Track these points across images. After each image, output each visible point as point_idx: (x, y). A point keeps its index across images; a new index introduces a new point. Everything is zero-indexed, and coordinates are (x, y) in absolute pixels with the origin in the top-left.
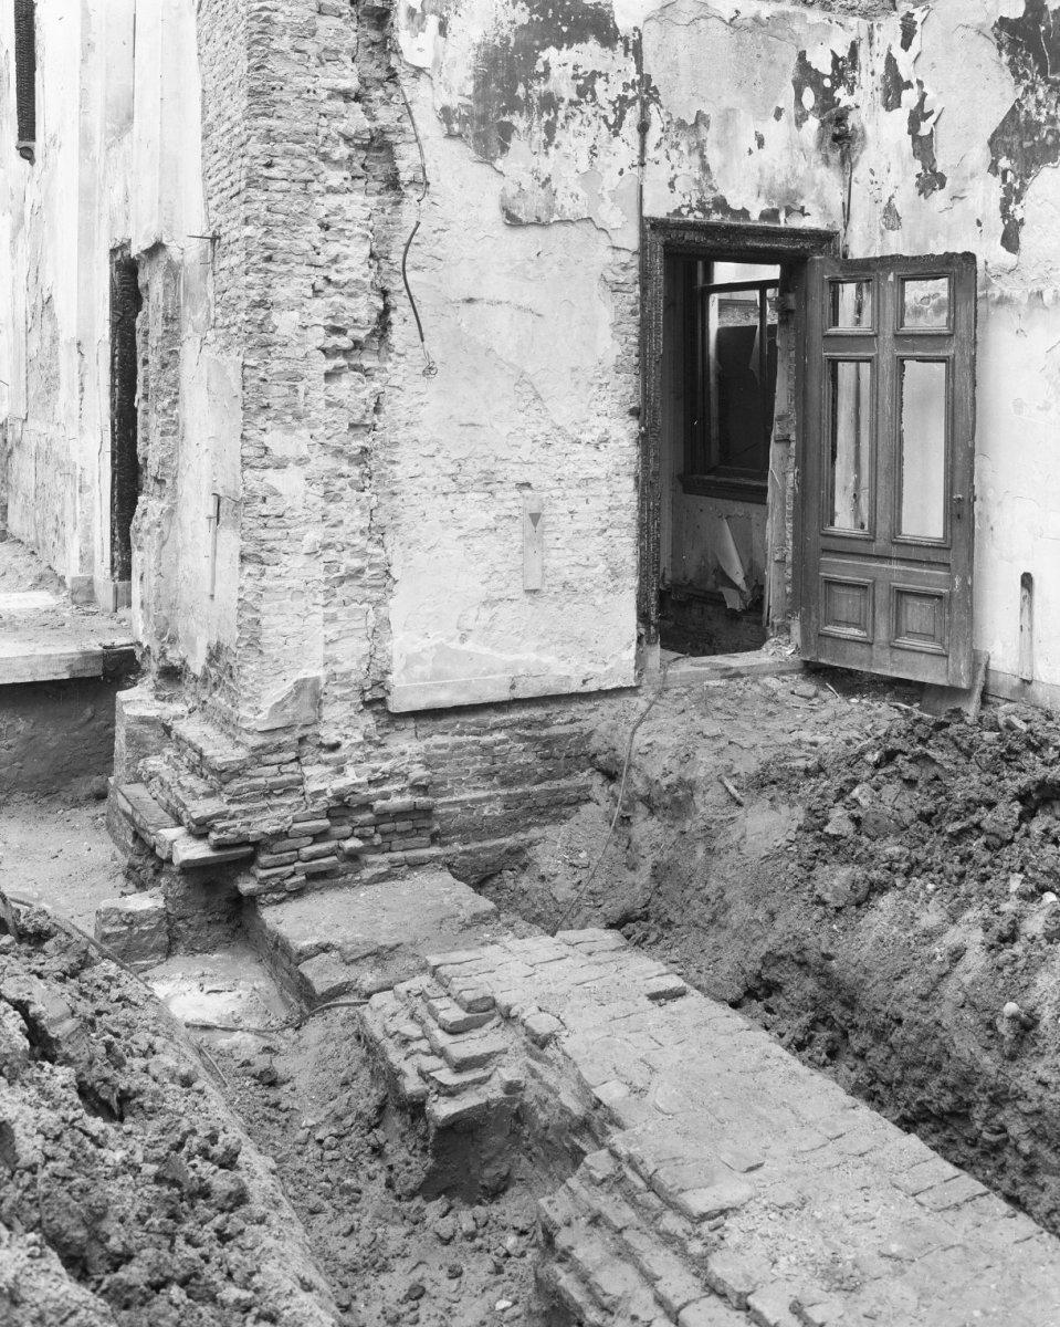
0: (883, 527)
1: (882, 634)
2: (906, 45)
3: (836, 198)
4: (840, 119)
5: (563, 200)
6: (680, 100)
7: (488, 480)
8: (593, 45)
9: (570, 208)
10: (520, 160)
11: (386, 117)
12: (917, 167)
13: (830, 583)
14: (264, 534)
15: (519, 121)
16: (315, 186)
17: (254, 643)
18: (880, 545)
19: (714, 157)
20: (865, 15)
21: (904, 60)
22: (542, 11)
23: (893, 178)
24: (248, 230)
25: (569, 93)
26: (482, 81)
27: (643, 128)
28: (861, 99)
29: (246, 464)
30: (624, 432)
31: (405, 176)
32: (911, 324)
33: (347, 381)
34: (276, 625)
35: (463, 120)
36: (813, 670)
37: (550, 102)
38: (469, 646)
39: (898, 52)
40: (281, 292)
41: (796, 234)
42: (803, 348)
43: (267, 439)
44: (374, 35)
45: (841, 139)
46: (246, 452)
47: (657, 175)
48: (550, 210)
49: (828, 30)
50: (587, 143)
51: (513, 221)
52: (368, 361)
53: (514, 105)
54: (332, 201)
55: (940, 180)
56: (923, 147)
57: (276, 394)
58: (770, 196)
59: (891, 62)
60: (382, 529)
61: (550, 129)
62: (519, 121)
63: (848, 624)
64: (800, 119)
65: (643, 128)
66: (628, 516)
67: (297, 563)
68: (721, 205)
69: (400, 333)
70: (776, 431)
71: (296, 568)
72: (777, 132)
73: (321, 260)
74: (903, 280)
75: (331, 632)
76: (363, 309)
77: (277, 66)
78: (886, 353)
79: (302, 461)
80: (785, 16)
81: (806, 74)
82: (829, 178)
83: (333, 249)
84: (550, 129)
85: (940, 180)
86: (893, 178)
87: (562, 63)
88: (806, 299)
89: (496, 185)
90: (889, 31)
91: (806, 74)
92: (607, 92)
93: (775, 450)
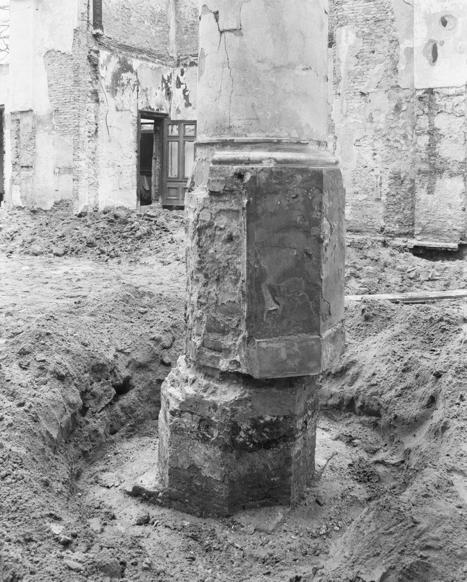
0: (181, 175)
1: (181, 197)
2: (182, 75)
3: (168, 107)
4: (168, 90)
5: (125, 106)
6: (143, 85)
7: (113, 165)
8: (130, 73)
9: (127, 107)
10: (119, 96)
11: (96, 87)
12: (185, 101)
13: (169, 188)
14: (78, 175)
15: (118, 88)
16: (86, 102)
17: (77, 198)
18: (180, 179)
19: (149, 98)
20: (172, 67)
21: (182, 79)
22: (122, 65)
23: (178, 103)
24: (75, 110)
25: (126, 83)
26: (113, 80)
27: (138, 91)
28: (172, 85)
29: (74, 160)
30: (134, 155)
31: (100, 100)
32: (187, 134)
33: (91, 143)
34: (81, 194)
35: (110, 88)
36: (164, 207)
37: (123, 85)
38: (110, 200)
39: (180, 76)
40: (82, 124)
41: (162, 114)
42: (162, 140)
43: (79, 154)
44: (94, 69)
45: (169, 94)
46: (74, 157)
47: (140, 100)
48: (123, 108)
49: (167, 70)
50: (129, 93)
51: (117, 110)
52: (93, 139)
53: (118, 85)
54: (89, 105)
55: (190, 105)
56: (186, 97)
57: (80, 145)
58: (158, 106)
59: (178, 78)
60: (97, 175)
61: (123, 90)
62: (118, 88)
63: (173, 196)
64: (162, 90)
65: (138, 91)
66: (135, 173)
67: (84, 181)
68: (150, 107)
69: (102, 131)
70: (154, 157)
71: (84, 182)
72: (159, 92)
73: (87, 117)
74: (185, 125)
75: (90, 195)
76: (94, 128)
77: (81, 76)
78: (181, 140)
79: (85, 159)
80: (160, 67)
81: (163, 80)
82: (167, 102)
83: (89, 115)
84: (123, 90)
85: (190, 105)
86: (178, 103)
87: (125, 76)
88: (163, 128)
89: (114, 102)
90: (178, 72)
91: (163, 80)
92: (132, 83)
93: (153, 161)
